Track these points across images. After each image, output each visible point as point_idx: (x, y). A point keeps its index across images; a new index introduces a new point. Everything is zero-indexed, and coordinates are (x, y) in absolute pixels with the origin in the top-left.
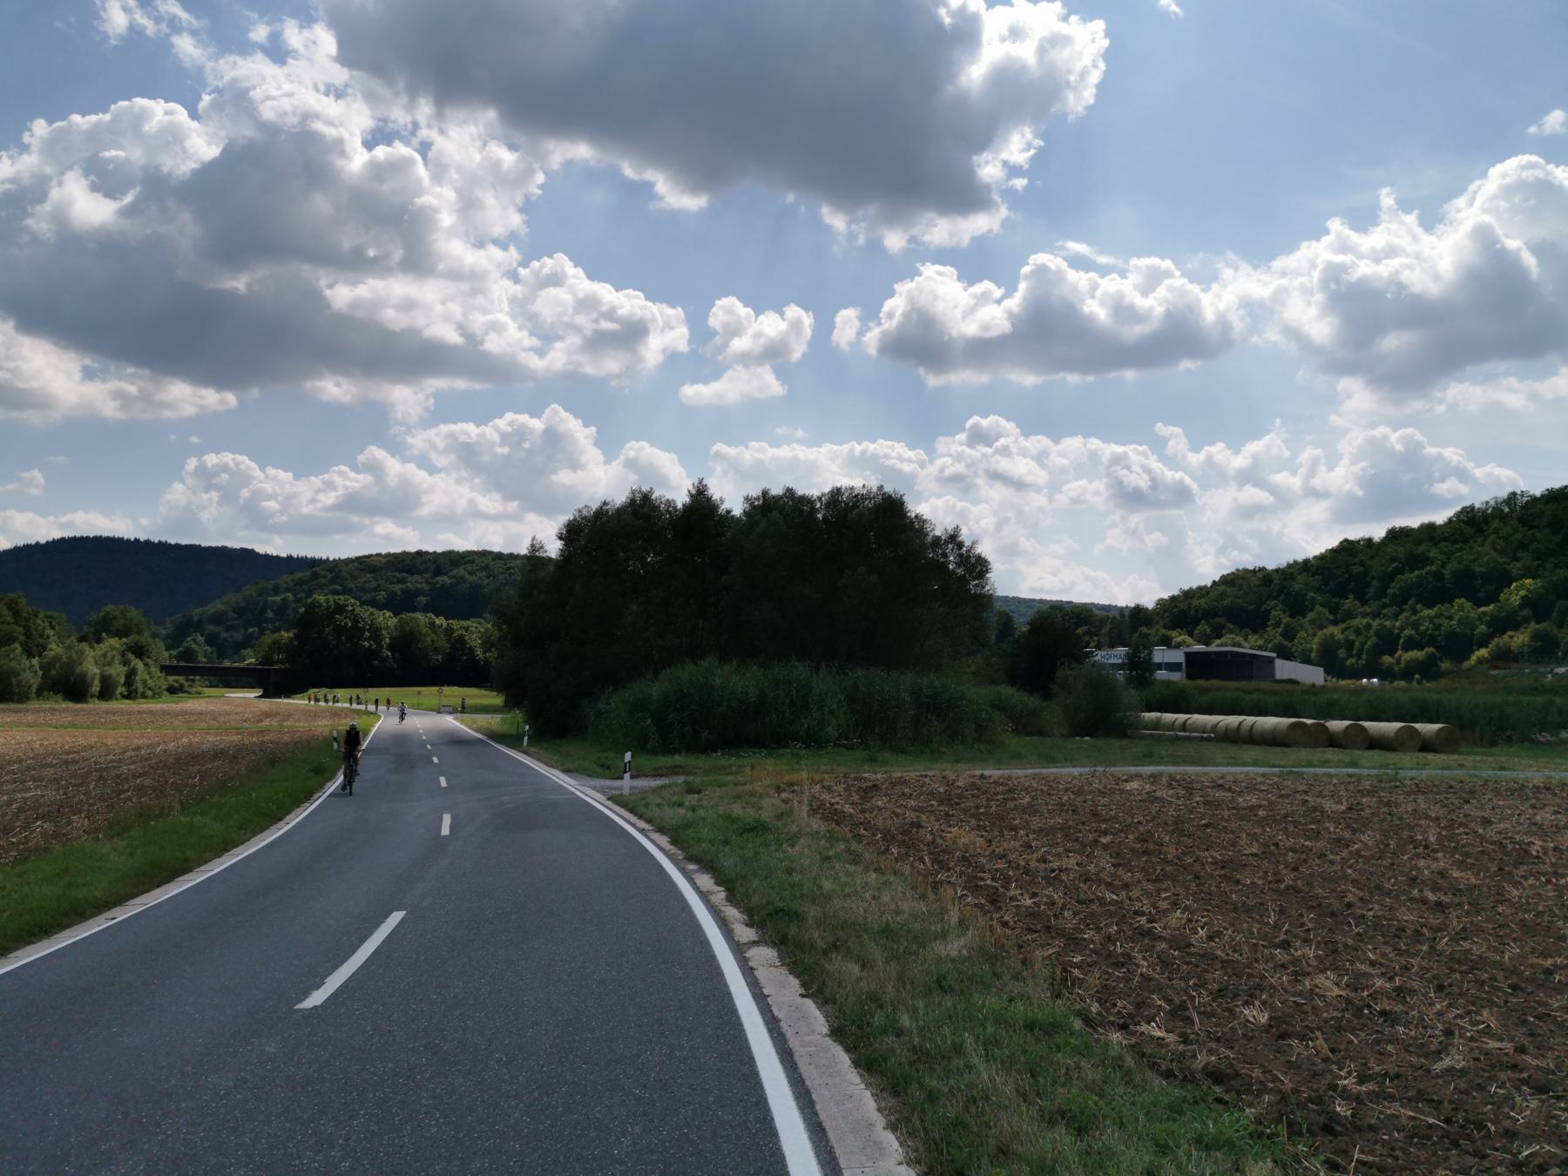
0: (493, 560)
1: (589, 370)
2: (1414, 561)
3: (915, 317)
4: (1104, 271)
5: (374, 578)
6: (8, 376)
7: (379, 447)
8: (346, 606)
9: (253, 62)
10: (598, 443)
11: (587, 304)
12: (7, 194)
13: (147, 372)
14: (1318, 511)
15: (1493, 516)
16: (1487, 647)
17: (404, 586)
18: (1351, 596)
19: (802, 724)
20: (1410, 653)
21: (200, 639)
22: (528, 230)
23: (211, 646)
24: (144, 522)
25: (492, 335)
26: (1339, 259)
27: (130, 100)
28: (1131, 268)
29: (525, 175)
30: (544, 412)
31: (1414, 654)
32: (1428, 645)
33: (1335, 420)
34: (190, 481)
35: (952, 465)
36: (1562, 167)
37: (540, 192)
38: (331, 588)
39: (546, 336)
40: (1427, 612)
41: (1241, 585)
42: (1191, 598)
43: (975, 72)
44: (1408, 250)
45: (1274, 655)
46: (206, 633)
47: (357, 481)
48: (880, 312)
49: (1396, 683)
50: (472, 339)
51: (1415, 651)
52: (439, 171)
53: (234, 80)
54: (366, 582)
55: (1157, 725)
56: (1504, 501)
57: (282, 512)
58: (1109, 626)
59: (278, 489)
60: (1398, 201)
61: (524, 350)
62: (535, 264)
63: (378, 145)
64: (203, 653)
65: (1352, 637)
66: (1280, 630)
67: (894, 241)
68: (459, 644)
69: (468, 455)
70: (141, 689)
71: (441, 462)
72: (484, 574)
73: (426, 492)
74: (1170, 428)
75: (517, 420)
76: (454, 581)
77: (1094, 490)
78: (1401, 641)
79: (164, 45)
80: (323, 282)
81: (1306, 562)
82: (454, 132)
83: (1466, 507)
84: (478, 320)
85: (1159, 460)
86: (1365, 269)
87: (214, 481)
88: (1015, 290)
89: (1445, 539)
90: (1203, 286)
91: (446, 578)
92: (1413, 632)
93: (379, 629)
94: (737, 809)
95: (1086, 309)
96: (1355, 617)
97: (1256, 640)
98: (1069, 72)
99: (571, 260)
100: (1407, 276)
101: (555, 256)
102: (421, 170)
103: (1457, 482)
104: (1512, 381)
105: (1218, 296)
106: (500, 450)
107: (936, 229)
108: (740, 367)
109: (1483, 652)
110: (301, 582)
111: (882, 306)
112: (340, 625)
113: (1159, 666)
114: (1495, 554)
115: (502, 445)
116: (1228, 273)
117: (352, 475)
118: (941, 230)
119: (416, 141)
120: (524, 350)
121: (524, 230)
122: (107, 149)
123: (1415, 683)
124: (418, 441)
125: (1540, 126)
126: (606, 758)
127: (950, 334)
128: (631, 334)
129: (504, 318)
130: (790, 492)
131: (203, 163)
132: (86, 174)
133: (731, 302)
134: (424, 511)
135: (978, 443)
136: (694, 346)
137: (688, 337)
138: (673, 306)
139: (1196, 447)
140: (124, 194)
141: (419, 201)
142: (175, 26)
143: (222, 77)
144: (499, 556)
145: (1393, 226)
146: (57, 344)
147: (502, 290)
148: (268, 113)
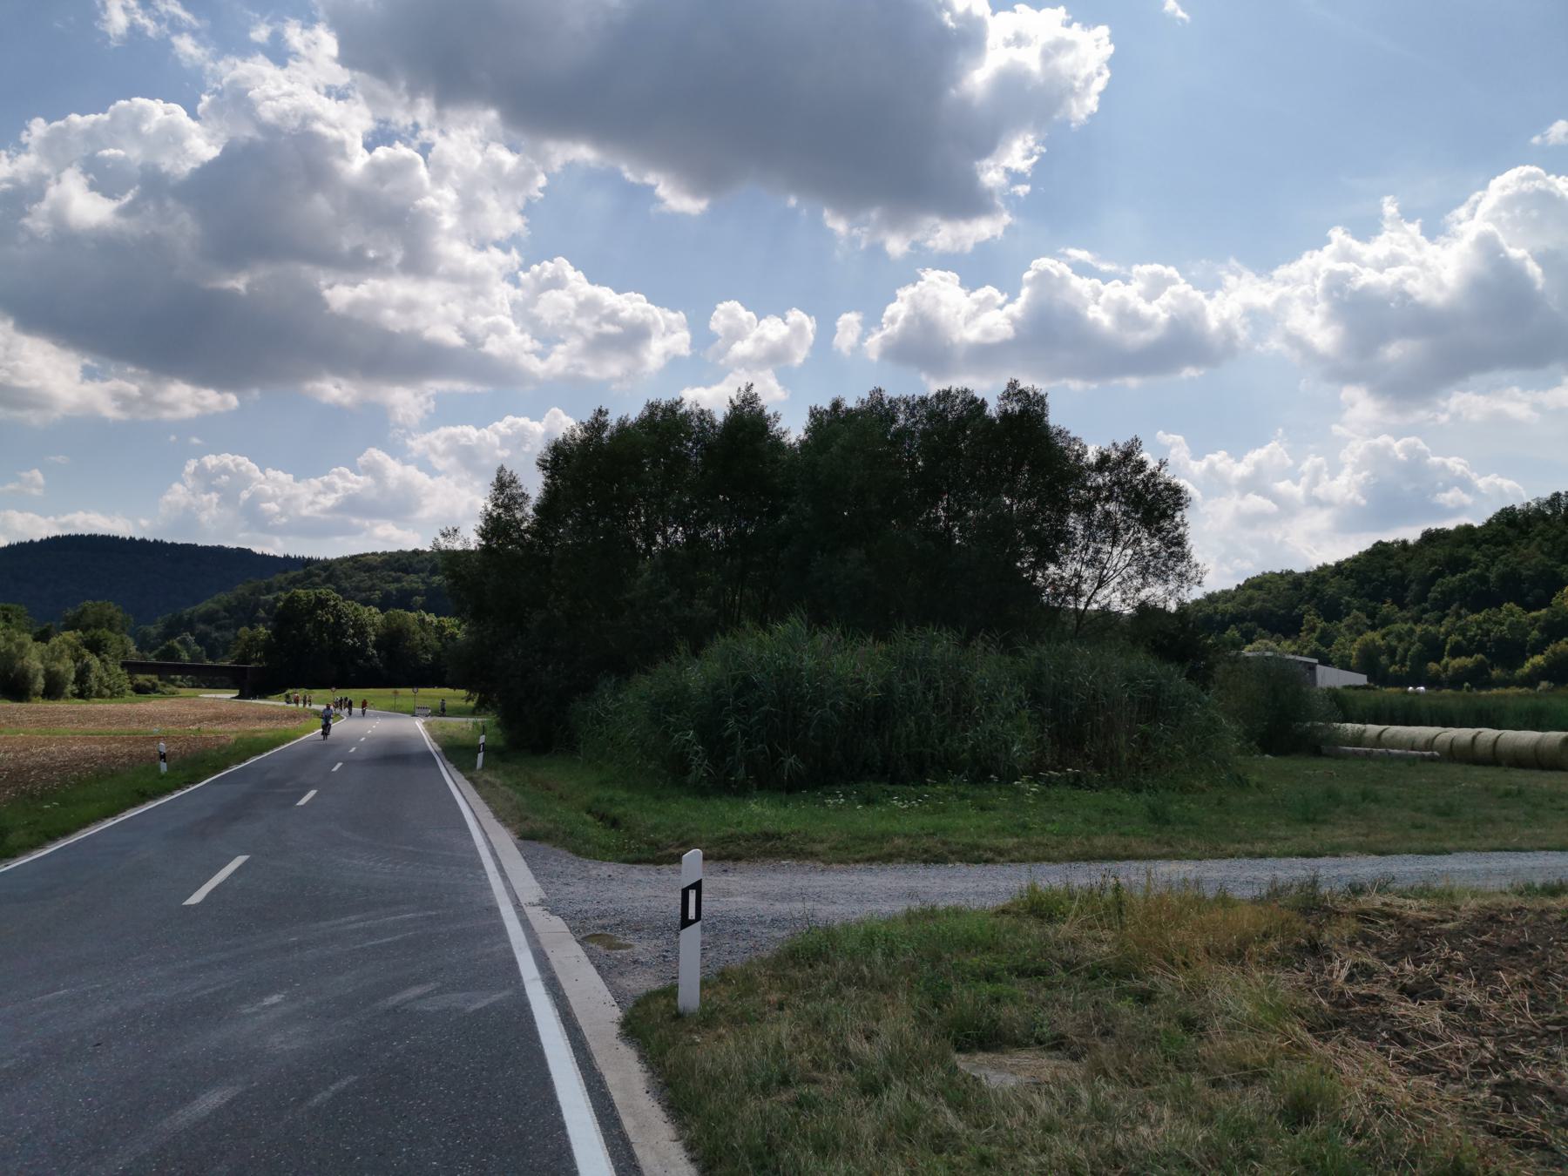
1: (590, 373)
2: (1456, 564)
4: (1106, 278)
5: (369, 577)
6: (6, 374)
8: (328, 600)
9: (254, 63)
11: (588, 306)
12: (6, 193)
13: (147, 372)
14: (1321, 520)
16: (1542, 654)
17: (399, 585)
18: (1389, 600)
19: (964, 740)
20: (1458, 660)
21: (191, 638)
22: (529, 233)
24: (144, 522)
25: (493, 337)
27: (129, 100)
28: (1134, 276)
33: (1337, 429)
34: (190, 483)
36: (1563, 177)
37: (541, 195)
39: (547, 338)
40: (1471, 618)
41: (1270, 589)
42: (1217, 602)
43: (979, 78)
44: (1412, 260)
45: (1316, 661)
47: (357, 483)
48: (882, 317)
49: (1444, 691)
50: (474, 341)
51: (1463, 658)
52: (440, 173)
53: (234, 82)
55: (1358, 740)
56: (1548, 502)
57: (282, 514)
59: (278, 491)
60: (1400, 210)
61: (526, 353)
62: (536, 268)
63: (378, 146)
65: (1394, 643)
66: (1315, 635)
67: (896, 245)
70: (96, 687)
71: (440, 464)
74: (1172, 436)
75: (518, 423)
78: (1448, 647)
79: (165, 46)
80: (323, 283)
83: (1506, 509)
84: (479, 322)
86: (1368, 277)
87: (213, 483)
88: (1018, 295)
89: (1486, 541)
90: (1208, 293)
92: (1460, 638)
93: (363, 626)
95: (1090, 315)
96: (1394, 622)
97: (1290, 646)
98: (1074, 77)
100: (1412, 286)
101: (555, 260)
102: (423, 172)
103: (1461, 492)
104: (1516, 390)
108: (742, 371)
109: (1538, 659)
111: (884, 311)
114: (1542, 557)
115: (502, 447)
116: (1231, 280)
117: (352, 476)
118: (945, 234)
119: (416, 143)
120: (526, 353)
121: (526, 233)
122: (106, 147)
123: (1465, 691)
124: (417, 444)
126: (611, 800)
128: (634, 336)
132: (85, 172)
133: (734, 305)
137: (689, 341)
138: (674, 310)
139: (1198, 456)
140: (124, 193)
142: (176, 27)
143: (221, 78)
145: (1396, 235)
146: (55, 343)
147: (503, 293)
148: (267, 112)
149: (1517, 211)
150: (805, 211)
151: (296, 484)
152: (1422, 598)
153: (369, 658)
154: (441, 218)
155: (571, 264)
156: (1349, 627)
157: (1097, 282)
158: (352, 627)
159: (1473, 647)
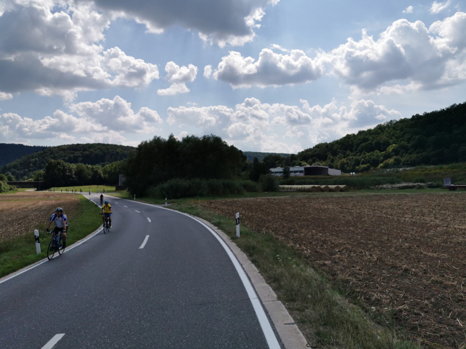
1: (128, 84)
2: (365, 140)
3: (228, 68)
4: (284, 54)
7: (60, 110)
10: (132, 108)
11: (126, 63)
15: (386, 127)
25: (96, 74)
26: (351, 50)
35: (241, 113)
37: (109, 27)
40: (368, 154)
45: (328, 167)
46: (12, 171)
47: (53, 121)
52: (76, 21)
55: (283, 188)
57: (30, 132)
58: (285, 160)
59: (28, 124)
60: (367, 32)
61: (106, 78)
62: (109, 50)
64: (14, 180)
65: (348, 161)
66: (330, 160)
67: (222, 44)
68: (96, 173)
69: (90, 112)
70: (3, 190)
71: (81, 114)
72: (99, 150)
73: (76, 124)
77: (282, 119)
78: (361, 162)
80: (40, 57)
81: (337, 141)
82: (81, 8)
84: (91, 69)
85: (301, 110)
86: (358, 53)
87: (7, 122)
88: (258, 59)
89: (373, 134)
91: (87, 152)
94: (188, 206)
95: (278, 65)
96: (349, 156)
99: (120, 49)
101: (115, 47)
102: (70, 20)
104: (398, 86)
105: (316, 61)
107: (234, 40)
108: (175, 84)
109: (382, 165)
110: (40, 155)
111: (218, 64)
113: (292, 172)
115: (101, 109)
116: (319, 54)
117: (52, 119)
118: (235, 41)
119: (68, 11)
120: (106, 78)
121: (104, 40)
124: (73, 107)
125: (406, 10)
127: (239, 73)
128: (141, 73)
129: (98, 68)
130: (193, 136)
134: (76, 130)
137: (158, 74)
138: (153, 64)
139: (311, 106)
141: (70, 31)
144: (104, 145)
145: (366, 40)
149: (400, 31)
152: (357, 149)
153: (73, 178)
156: (339, 158)
157: (281, 55)
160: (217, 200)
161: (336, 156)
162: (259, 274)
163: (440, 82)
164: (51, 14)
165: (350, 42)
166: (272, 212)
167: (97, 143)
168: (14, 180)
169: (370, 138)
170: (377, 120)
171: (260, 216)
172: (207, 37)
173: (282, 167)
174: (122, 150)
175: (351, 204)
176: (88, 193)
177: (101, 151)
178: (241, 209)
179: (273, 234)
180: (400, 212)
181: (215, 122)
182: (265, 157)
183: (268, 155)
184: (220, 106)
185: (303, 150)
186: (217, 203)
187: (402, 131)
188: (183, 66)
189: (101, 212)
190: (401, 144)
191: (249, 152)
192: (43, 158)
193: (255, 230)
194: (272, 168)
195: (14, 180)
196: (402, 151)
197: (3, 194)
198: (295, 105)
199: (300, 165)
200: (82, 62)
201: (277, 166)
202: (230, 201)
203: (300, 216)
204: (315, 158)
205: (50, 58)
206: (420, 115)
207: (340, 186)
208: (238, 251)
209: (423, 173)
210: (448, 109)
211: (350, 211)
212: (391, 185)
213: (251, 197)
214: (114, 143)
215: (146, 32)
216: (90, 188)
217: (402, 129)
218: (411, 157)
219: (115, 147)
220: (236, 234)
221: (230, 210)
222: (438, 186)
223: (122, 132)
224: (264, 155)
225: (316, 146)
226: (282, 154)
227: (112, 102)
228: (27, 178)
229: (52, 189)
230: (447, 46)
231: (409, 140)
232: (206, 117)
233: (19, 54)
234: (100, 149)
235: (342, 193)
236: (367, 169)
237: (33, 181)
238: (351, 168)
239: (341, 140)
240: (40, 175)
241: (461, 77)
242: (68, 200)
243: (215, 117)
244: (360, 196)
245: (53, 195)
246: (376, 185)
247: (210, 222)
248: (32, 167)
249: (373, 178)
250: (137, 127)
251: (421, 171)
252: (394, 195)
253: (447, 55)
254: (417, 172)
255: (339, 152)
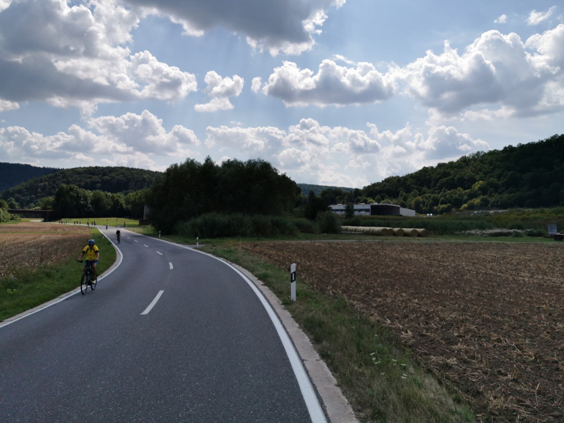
0: (126, 170)
1: (159, 97)
2: (446, 175)
3: (281, 81)
4: (349, 66)
7: (76, 125)
10: (163, 125)
11: (157, 71)
22: (133, 41)
23: (18, 202)
25: (120, 82)
29: (131, 20)
30: (142, 113)
31: (444, 206)
32: (448, 203)
35: (295, 136)
36: (505, 35)
37: (138, 26)
38: (62, 180)
40: (449, 192)
42: (375, 186)
44: (453, 63)
45: (400, 206)
46: (15, 197)
47: (68, 138)
49: (438, 215)
50: (112, 84)
51: (444, 205)
52: (98, 17)
54: (76, 178)
55: (346, 230)
56: (476, 155)
57: (39, 150)
58: (347, 196)
59: (37, 141)
60: (450, 45)
61: (133, 88)
62: (137, 54)
64: (17, 207)
65: (425, 200)
66: (402, 197)
67: (274, 52)
68: (117, 202)
69: (112, 129)
71: (101, 131)
72: (122, 175)
75: (132, 116)
76: (111, 178)
77: (345, 146)
78: (440, 201)
80: (53, 60)
81: (412, 174)
84: (114, 76)
86: (438, 69)
87: (12, 137)
88: (318, 72)
89: (456, 167)
91: (107, 177)
92: (444, 198)
94: (225, 249)
95: (342, 81)
96: (426, 193)
97: (395, 201)
101: (145, 51)
102: (91, 16)
104: (486, 110)
105: (388, 77)
106: (125, 127)
107: (289, 48)
108: (217, 98)
109: (465, 205)
110: (51, 178)
112: (72, 195)
113: (356, 210)
115: (125, 125)
116: (391, 69)
117: (66, 136)
118: (290, 48)
119: (89, 5)
120: (133, 88)
121: (132, 41)
124: (92, 122)
125: (498, 20)
127: (294, 89)
128: (175, 84)
129: (124, 75)
130: (235, 160)
131: (2, 10)
134: (95, 150)
135: (304, 129)
136: (199, 89)
137: (197, 86)
138: (191, 73)
139: (380, 132)
144: (128, 169)
145: (449, 54)
149: (490, 46)
150: (239, 37)
151: (44, 138)
152: (435, 185)
153: (89, 208)
154: (99, 34)
155: (151, 53)
156: (413, 195)
157: (345, 68)
158: (83, 197)
159: (447, 201)
160: (263, 242)
161: (410, 192)
162: (339, 390)
163: (537, 108)
164: (68, 8)
165: (430, 56)
166: (337, 261)
167: (120, 166)
168: (17, 207)
169: (451, 172)
170: (459, 152)
171: (321, 267)
172: (256, 42)
173: (343, 203)
174: (149, 176)
175: (439, 254)
176: (105, 227)
177: (124, 177)
178: (295, 255)
179: (345, 297)
180: (510, 268)
181: (263, 146)
182: (323, 191)
183: (327, 188)
184: (269, 127)
185: (369, 184)
186: (263, 246)
187: (491, 165)
188: (226, 77)
189: (80, 259)
190: (489, 181)
191: (304, 184)
192: (54, 182)
193: (317, 288)
194: (331, 204)
195: (18, 208)
196: (492, 189)
197: (3, 224)
198: (361, 130)
199: (366, 202)
200: (104, 68)
201: (338, 202)
202: (280, 244)
203: (376, 269)
204: (384, 194)
205: (65, 61)
206: (514, 146)
207: (417, 229)
208: (294, 327)
209: (520, 217)
210: (547, 141)
211: (441, 263)
212: (480, 231)
213: (307, 239)
214: (140, 168)
215: (182, 34)
216: (107, 220)
217: (491, 163)
218: (501, 198)
219: (142, 171)
220: (290, 295)
221: (280, 256)
222: (539, 235)
223: (151, 154)
224: (322, 189)
225: (386, 179)
226: (344, 188)
227: (139, 118)
228: (34, 206)
229: (63, 220)
230: (547, 64)
231: (499, 177)
232: (253, 140)
233: (28, 55)
234: (123, 173)
235: (421, 238)
236: (448, 210)
237: (40, 210)
238: (428, 208)
239: (416, 173)
240: (48, 203)
241: (562, 102)
242: (77, 234)
243: (264, 141)
244: (448, 244)
245: (62, 228)
246: (462, 230)
247: (253, 274)
248: (40, 193)
249: (458, 221)
250: (169, 149)
251: (517, 215)
252: (491, 243)
253: (546, 76)
254: (513, 216)
255: (413, 188)
